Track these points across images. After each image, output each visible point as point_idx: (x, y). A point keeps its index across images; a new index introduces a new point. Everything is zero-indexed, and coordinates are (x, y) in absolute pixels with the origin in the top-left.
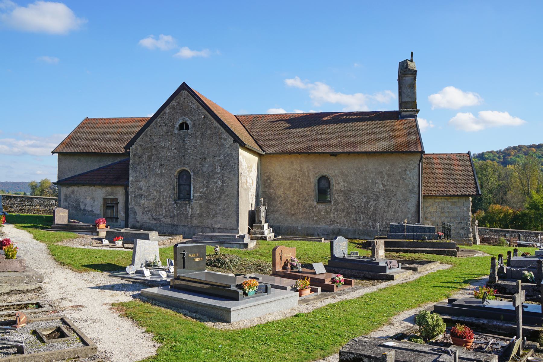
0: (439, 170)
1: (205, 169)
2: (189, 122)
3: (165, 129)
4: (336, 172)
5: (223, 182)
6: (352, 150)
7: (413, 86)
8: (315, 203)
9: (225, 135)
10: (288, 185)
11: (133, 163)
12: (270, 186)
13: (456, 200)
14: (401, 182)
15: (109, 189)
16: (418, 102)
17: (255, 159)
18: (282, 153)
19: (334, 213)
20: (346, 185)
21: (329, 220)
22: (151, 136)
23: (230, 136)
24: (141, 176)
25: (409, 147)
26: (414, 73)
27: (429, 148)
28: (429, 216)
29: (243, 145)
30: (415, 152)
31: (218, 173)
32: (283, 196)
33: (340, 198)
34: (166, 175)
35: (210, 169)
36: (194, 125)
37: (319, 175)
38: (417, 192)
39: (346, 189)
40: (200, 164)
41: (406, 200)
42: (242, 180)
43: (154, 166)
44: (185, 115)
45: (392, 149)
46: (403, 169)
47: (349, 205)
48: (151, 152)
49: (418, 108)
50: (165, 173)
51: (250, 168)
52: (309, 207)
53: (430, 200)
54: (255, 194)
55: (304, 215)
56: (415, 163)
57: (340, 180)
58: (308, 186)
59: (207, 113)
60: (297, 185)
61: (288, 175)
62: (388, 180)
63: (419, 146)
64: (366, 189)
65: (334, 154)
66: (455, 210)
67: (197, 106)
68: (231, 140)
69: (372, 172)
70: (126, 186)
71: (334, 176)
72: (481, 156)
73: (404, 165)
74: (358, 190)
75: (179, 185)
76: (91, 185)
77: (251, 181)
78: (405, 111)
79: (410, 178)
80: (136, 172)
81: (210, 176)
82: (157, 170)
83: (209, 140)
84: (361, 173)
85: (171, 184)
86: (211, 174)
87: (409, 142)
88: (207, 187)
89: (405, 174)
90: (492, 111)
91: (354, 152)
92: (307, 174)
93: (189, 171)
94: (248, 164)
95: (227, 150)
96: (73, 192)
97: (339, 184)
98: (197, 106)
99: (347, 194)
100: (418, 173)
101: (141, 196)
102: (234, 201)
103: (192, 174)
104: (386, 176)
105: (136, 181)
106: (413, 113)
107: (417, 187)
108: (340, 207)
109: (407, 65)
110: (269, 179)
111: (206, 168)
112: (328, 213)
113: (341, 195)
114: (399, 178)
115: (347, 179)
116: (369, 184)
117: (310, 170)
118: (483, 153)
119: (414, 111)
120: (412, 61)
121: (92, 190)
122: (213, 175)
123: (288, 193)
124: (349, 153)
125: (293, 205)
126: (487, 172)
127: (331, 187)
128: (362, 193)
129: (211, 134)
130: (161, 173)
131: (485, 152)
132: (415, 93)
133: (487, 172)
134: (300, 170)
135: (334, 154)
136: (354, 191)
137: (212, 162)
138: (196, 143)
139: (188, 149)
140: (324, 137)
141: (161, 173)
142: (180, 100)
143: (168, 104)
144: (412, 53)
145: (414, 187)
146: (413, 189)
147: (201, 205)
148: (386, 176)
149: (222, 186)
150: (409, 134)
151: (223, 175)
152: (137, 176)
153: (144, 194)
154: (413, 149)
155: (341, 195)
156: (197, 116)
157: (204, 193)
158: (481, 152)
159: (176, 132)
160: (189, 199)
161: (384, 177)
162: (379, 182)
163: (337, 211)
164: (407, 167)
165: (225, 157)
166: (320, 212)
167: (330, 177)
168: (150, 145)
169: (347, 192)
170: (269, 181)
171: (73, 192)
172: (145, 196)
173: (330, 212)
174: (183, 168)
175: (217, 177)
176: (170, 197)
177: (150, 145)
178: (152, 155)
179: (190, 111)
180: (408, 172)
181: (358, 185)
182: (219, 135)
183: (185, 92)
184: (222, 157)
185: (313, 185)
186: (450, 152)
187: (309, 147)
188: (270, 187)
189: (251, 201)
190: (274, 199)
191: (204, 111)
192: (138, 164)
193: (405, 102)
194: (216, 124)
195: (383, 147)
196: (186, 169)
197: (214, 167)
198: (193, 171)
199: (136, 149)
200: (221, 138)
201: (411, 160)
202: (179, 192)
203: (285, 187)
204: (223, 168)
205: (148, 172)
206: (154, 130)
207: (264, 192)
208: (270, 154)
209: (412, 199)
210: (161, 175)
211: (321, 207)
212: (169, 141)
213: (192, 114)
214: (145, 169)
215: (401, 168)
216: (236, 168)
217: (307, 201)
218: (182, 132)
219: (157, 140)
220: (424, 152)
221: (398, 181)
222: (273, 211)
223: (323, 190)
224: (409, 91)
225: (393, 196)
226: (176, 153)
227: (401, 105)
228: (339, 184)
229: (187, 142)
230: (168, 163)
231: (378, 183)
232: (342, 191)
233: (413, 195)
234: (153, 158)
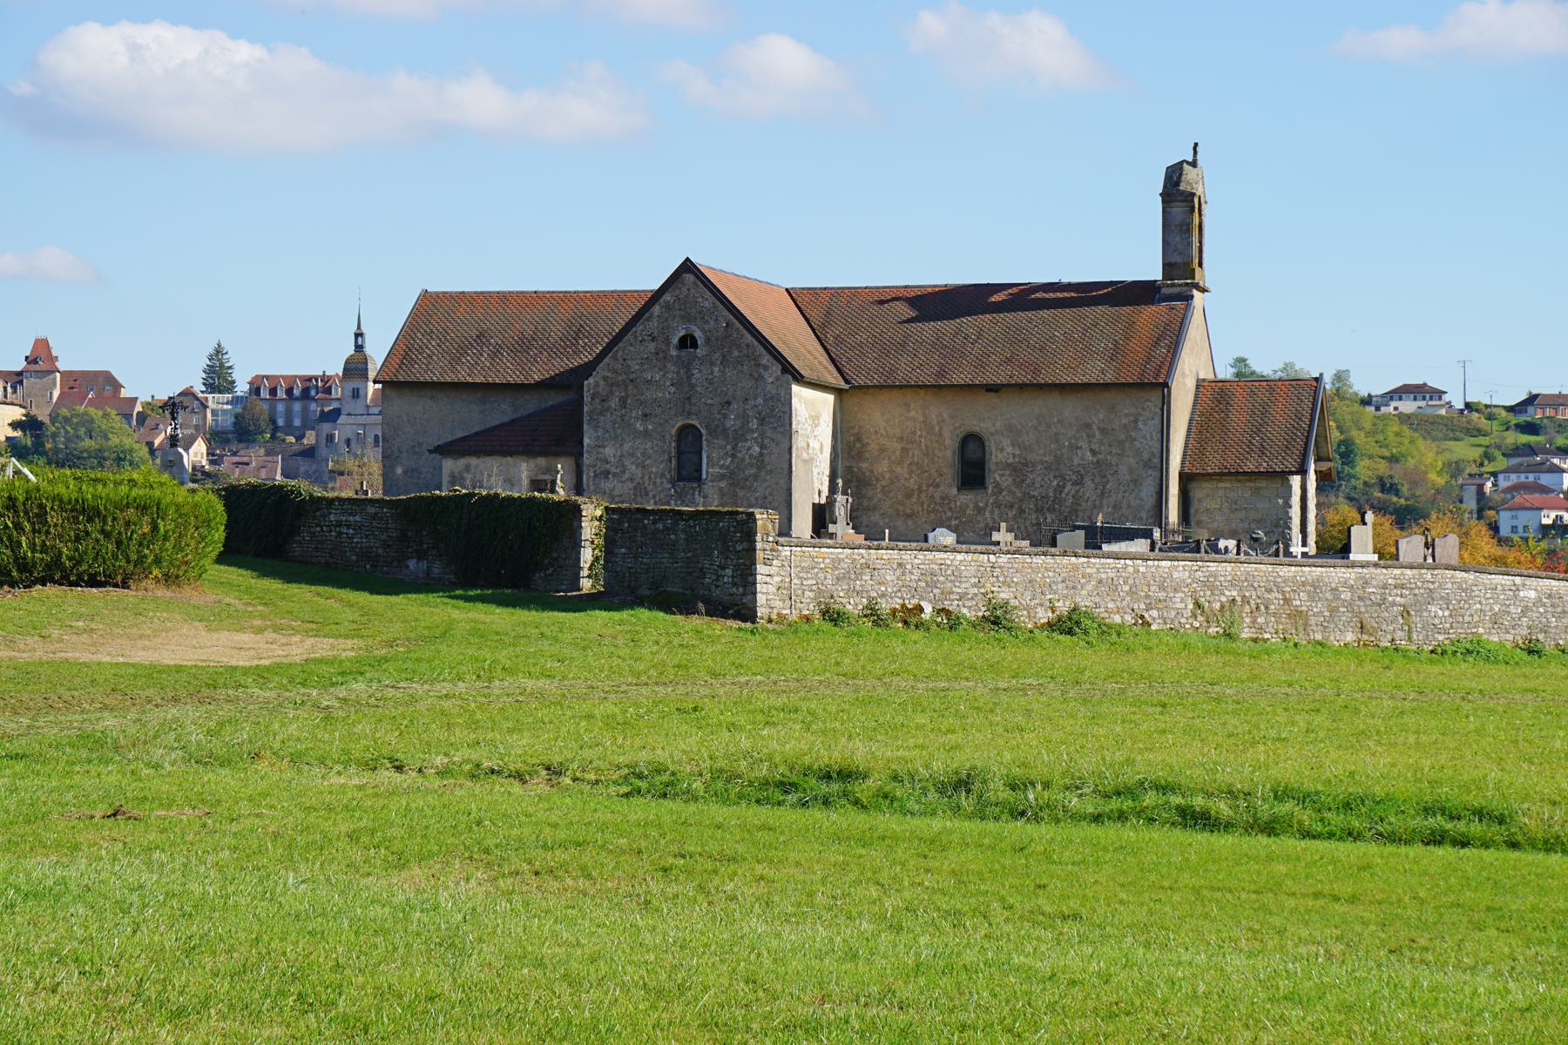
1: (729, 423)
2: (698, 334)
3: (652, 346)
5: (762, 447)
6: (1026, 378)
8: (955, 491)
9: (766, 359)
11: (591, 413)
12: (860, 456)
13: (1262, 484)
14: (1127, 445)
15: (541, 461)
17: (830, 398)
18: (881, 387)
19: (992, 512)
21: (982, 525)
28: (1205, 518)
29: (799, 379)
31: (753, 431)
33: (1006, 481)
35: (739, 423)
36: (708, 340)
37: (961, 433)
41: (1136, 482)
42: (798, 443)
44: (689, 321)
47: (1024, 494)
51: (815, 419)
52: (943, 498)
53: (1205, 485)
54: (827, 472)
55: (932, 516)
57: (1006, 442)
66: (1260, 505)
68: (777, 368)
70: (578, 456)
73: (1133, 410)
74: (1042, 462)
75: (680, 453)
77: (817, 446)
79: (1144, 437)
80: (596, 428)
81: (740, 436)
88: (733, 456)
90: (372, 593)
94: (813, 415)
95: (769, 387)
99: (1019, 470)
101: (606, 474)
102: (782, 482)
103: (704, 432)
108: (1005, 497)
110: (859, 440)
111: (731, 422)
112: (980, 511)
120: (1194, 164)
124: (1022, 387)
125: (909, 496)
128: (1048, 468)
130: (646, 431)
136: (1034, 465)
141: (646, 431)
147: (721, 489)
149: (761, 454)
151: (762, 435)
153: (613, 470)
157: (728, 467)
159: (674, 352)
160: (699, 479)
163: (999, 506)
166: (963, 508)
167: (985, 435)
172: (615, 475)
173: (984, 509)
176: (662, 475)
178: (627, 397)
180: (1140, 425)
183: (689, 278)
184: (760, 400)
185: (949, 453)
187: (940, 374)
189: (817, 485)
190: (869, 484)
191: (727, 313)
192: (601, 414)
194: (749, 338)
195: (1093, 371)
197: (745, 418)
199: (597, 385)
200: (758, 365)
202: (679, 467)
204: (762, 421)
207: (849, 469)
208: (860, 387)
209: (1149, 481)
210: (646, 434)
211: (967, 498)
214: (614, 422)
215: (1127, 415)
217: (938, 486)
221: (1121, 443)
222: (868, 509)
223: (972, 468)
227: (1168, 267)
230: (658, 411)
232: (1009, 465)
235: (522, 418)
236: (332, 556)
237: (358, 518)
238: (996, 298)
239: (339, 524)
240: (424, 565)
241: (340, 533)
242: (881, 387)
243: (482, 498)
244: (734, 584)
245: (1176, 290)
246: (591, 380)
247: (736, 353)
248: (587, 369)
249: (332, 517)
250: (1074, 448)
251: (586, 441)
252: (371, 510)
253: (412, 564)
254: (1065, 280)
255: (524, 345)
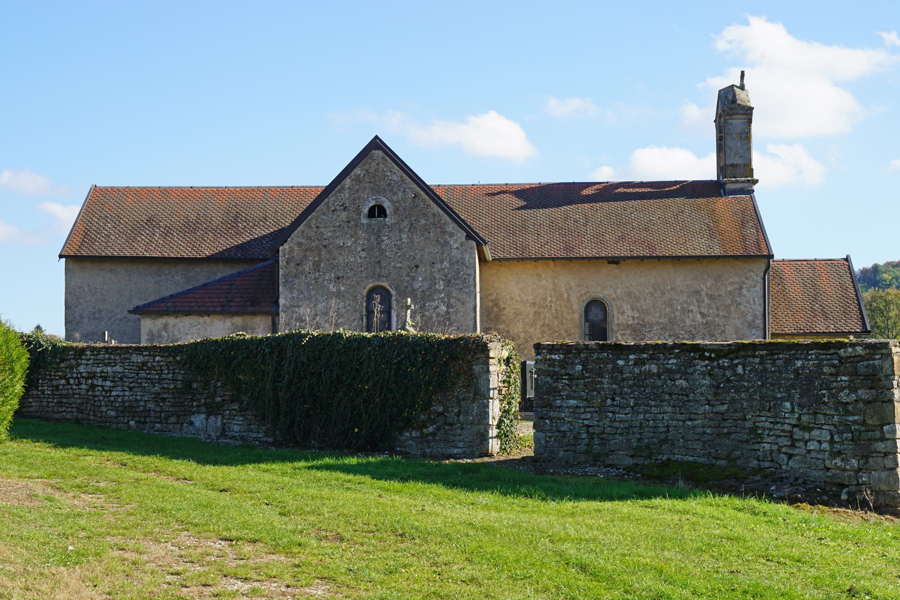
0: (795, 291)
1: (417, 285)
2: (387, 205)
3: (344, 215)
4: (619, 291)
6: (646, 253)
7: (746, 136)
9: (452, 227)
10: (531, 316)
11: (286, 276)
14: (732, 308)
15: (238, 320)
16: (755, 165)
18: (518, 260)
20: (636, 315)
22: (318, 227)
23: (459, 229)
24: (302, 296)
25: (745, 248)
26: (748, 112)
27: (779, 254)
30: (757, 256)
31: (440, 292)
32: (522, 335)
34: (347, 295)
36: (396, 210)
37: (587, 299)
38: (762, 326)
39: (636, 322)
40: (408, 275)
43: (324, 279)
44: (379, 193)
45: (717, 251)
46: (737, 286)
48: (319, 255)
49: (755, 177)
50: (346, 291)
56: (757, 275)
57: (626, 307)
58: (569, 317)
59: (418, 189)
60: (547, 315)
61: (531, 297)
62: (709, 306)
63: (763, 246)
64: (672, 321)
65: (614, 261)
67: (401, 177)
69: (682, 291)
71: (614, 300)
72: (872, 276)
73: (737, 279)
74: (658, 323)
76: (200, 313)
78: (733, 182)
79: (748, 302)
80: (291, 289)
82: (331, 287)
83: (422, 235)
84: (663, 293)
85: (356, 311)
86: (428, 293)
87: (744, 239)
89: (740, 295)
91: (651, 257)
92: (565, 295)
93: (389, 288)
95: (454, 252)
96: (165, 327)
97: (623, 313)
98: (401, 177)
100: (762, 294)
103: (393, 292)
104: (706, 299)
105: (291, 306)
106: (746, 185)
107: (760, 317)
109: (734, 95)
110: (496, 305)
113: (628, 332)
114: (729, 302)
115: (638, 305)
116: (678, 314)
117: (570, 289)
118: (876, 268)
119: (749, 181)
120: (742, 87)
121: (205, 322)
122: (430, 295)
123: (532, 330)
124: (643, 258)
126: (889, 318)
127: (609, 318)
128: (664, 329)
129: (426, 225)
130: (339, 292)
131: (881, 262)
132: (749, 149)
133: (889, 318)
134: (554, 289)
135: (614, 261)
136: (651, 325)
137: (428, 272)
138: (401, 240)
139: (386, 250)
140: (591, 227)
141: (339, 292)
142: (370, 168)
143: (349, 174)
144: (743, 74)
145: (755, 316)
146: (753, 321)
148: (706, 299)
149: (447, 313)
150: (743, 224)
151: (449, 295)
152: (293, 297)
154: (754, 251)
155: (628, 332)
156: (400, 194)
158: (869, 265)
159: (364, 221)
161: (703, 301)
162: (695, 309)
164: (743, 282)
165: (451, 264)
168: (317, 243)
169: (639, 327)
170: (495, 309)
171: (165, 327)
174: (377, 283)
175: (439, 298)
177: (317, 243)
178: (320, 261)
179: (389, 185)
180: (744, 291)
181: (658, 315)
182: (441, 227)
183: (378, 153)
184: (446, 264)
185: (576, 316)
186: (813, 258)
187: (568, 248)
188: (497, 319)
192: (296, 276)
193: (733, 165)
194: (435, 208)
195: (700, 246)
196: (384, 284)
197: (433, 281)
198: (396, 288)
199: (292, 250)
201: (751, 270)
203: (527, 320)
204: (448, 283)
205: (313, 289)
206: (324, 217)
210: (338, 295)
212: (352, 236)
213: (392, 190)
214: (308, 284)
215: (731, 284)
216: (472, 283)
218: (374, 221)
219: (329, 234)
220: (772, 256)
221: (727, 307)
224: (739, 144)
225: (720, 334)
226: (365, 258)
227: (722, 169)
228: (623, 313)
229: (384, 238)
230: (350, 274)
231: (692, 311)
232: (628, 326)
233: (754, 331)
234: (322, 265)
235: (213, 283)
236: (80, 411)
237: (118, 368)
238: (585, 192)
239: (92, 376)
240: (216, 422)
241: (93, 386)
242: (518, 260)
243: (314, 338)
244: (835, 454)
245: (738, 186)
246: (286, 246)
247: (423, 222)
248: (282, 235)
249: (82, 369)
250: (686, 311)
251: (282, 301)
252: (137, 359)
253: (199, 420)
254: (645, 180)
255: (191, 227)
